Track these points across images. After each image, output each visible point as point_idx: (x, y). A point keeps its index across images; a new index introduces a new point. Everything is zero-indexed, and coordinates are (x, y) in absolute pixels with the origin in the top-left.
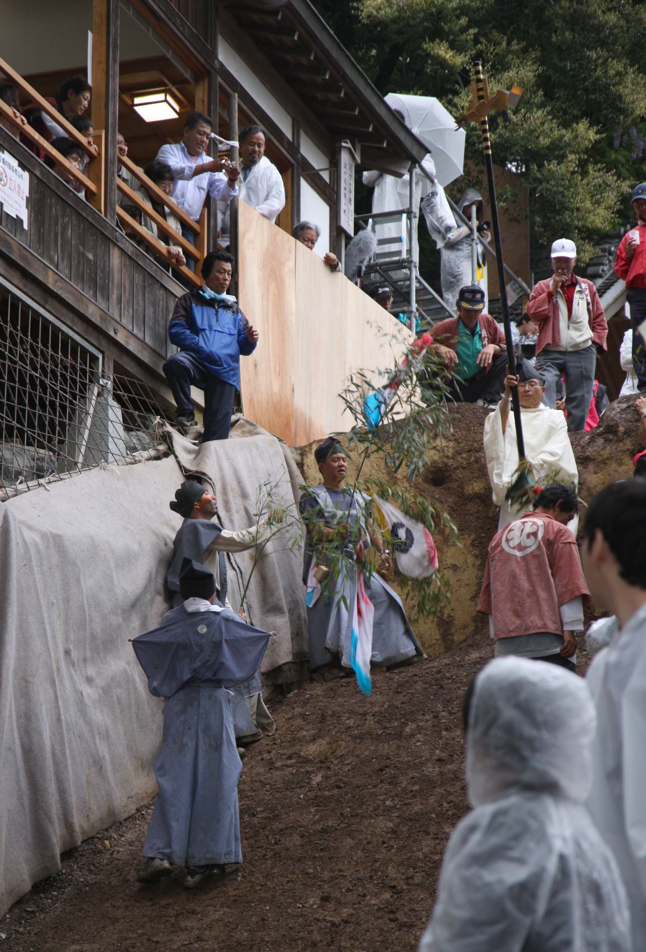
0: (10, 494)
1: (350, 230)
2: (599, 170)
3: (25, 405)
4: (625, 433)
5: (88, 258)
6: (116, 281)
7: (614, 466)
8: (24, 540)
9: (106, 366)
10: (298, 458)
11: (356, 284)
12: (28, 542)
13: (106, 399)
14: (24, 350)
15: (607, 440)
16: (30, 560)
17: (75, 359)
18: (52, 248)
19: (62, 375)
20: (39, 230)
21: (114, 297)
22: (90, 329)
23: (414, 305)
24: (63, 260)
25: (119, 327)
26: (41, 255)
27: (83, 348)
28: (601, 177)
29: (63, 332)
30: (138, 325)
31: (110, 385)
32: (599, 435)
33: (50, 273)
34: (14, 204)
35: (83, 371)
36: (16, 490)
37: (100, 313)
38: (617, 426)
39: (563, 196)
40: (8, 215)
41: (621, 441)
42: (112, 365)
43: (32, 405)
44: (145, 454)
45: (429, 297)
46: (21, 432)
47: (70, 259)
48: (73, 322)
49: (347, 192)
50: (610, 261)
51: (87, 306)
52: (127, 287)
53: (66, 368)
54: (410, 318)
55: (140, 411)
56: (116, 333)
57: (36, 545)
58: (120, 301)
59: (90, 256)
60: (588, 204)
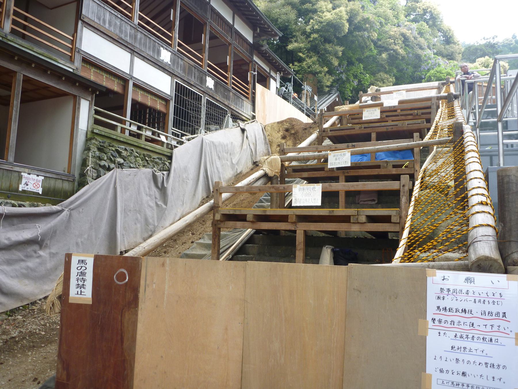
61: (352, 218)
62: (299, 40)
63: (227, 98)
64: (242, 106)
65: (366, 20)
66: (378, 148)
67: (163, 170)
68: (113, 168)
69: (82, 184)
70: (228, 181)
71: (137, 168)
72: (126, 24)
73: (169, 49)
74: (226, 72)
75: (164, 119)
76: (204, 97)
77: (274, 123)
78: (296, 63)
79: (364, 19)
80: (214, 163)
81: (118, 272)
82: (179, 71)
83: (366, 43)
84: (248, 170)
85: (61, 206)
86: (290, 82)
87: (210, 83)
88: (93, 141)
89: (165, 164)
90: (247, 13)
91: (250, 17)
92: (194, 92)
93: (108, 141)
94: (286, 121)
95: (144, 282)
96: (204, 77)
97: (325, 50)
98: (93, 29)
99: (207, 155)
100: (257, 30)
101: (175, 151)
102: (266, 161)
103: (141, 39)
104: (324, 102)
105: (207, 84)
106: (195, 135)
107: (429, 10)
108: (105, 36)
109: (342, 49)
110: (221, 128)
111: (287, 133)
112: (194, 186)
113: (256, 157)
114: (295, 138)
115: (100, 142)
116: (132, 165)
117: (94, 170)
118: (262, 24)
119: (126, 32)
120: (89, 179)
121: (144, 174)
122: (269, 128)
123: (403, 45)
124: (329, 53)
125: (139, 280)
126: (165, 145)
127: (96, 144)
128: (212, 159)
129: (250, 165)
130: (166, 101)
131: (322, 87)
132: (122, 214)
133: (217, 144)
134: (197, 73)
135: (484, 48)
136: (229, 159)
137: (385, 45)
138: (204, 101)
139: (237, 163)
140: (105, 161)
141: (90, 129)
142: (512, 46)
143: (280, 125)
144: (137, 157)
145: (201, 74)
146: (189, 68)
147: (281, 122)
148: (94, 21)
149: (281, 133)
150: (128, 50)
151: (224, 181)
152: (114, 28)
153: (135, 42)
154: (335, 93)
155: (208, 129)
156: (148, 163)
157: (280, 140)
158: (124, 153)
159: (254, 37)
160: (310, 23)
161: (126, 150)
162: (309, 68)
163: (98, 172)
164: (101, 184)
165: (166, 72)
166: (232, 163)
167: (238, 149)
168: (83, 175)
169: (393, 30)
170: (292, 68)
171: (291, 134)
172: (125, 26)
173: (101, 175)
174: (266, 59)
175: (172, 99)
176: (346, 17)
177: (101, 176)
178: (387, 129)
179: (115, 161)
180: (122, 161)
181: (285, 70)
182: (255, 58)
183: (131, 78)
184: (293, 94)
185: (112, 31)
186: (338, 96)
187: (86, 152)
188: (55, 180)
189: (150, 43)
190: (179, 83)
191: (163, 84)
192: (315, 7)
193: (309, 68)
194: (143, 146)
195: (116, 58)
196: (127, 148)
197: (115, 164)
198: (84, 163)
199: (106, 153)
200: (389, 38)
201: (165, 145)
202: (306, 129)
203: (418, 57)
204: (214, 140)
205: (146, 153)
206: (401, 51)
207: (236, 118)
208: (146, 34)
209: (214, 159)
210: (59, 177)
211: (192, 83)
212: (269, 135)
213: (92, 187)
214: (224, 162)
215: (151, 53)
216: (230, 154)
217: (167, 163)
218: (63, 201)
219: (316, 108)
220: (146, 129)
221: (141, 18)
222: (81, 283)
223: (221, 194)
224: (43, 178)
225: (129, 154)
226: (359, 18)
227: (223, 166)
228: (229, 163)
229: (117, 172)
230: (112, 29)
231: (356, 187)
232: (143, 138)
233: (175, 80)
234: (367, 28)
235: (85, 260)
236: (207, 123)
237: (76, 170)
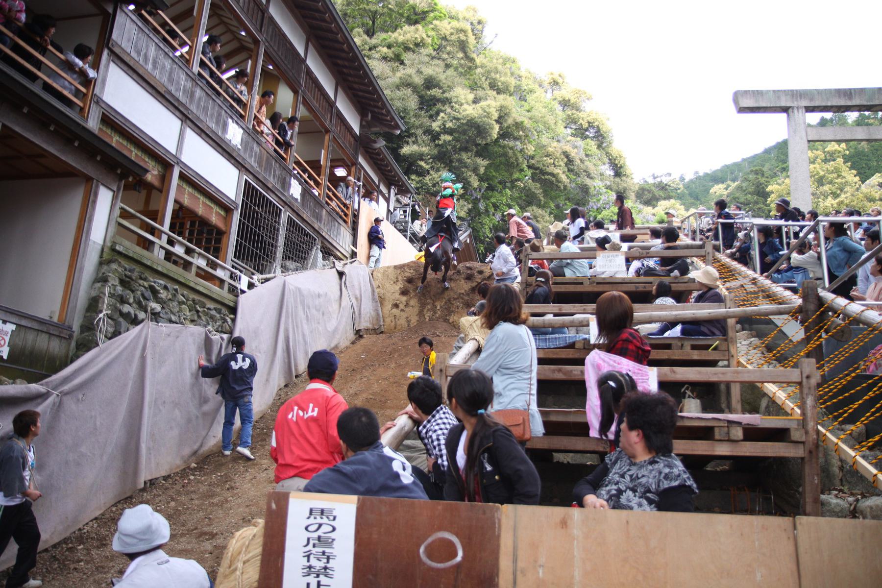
61: (717, 431)
62: (420, 141)
63: (318, 218)
64: (338, 234)
65: (519, 125)
66: (676, 315)
67: (222, 332)
68: (143, 321)
69: (86, 345)
71: (182, 323)
72: (181, 71)
73: (241, 124)
74: (319, 175)
75: (218, 241)
76: (285, 211)
77: (388, 267)
78: (413, 177)
79: (517, 123)
80: (300, 325)
81: (430, 540)
82: (252, 162)
83: (517, 159)
84: (348, 343)
85: (47, 384)
87: (296, 189)
88: (114, 266)
89: (225, 321)
90: (356, 86)
91: (361, 94)
92: (271, 202)
93: (138, 269)
95: (510, 564)
96: (288, 179)
97: (460, 161)
98: (126, 68)
100: (367, 116)
101: (242, 298)
103: (200, 99)
105: (292, 191)
106: (272, 275)
107: (596, 124)
108: (144, 85)
109: (485, 163)
110: (305, 268)
111: (410, 285)
112: (268, 365)
115: (125, 270)
116: (173, 318)
117: (110, 321)
118: (378, 107)
119: (178, 83)
120: (101, 337)
121: (192, 335)
123: (566, 170)
124: (466, 167)
125: (497, 559)
126: (226, 286)
127: (118, 272)
129: (351, 336)
130: (228, 210)
132: (150, 408)
134: (277, 170)
135: (653, 188)
137: (541, 166)
138: (284, 218)
140: (130, 304)
141: (109, 244)
142: (679, 191)
144: (183, 303)
145: (284, 172)
146: (267, 160)
147: (401, 268)
148: (129, 54)
149: (400, 285)
150: (177, 113)
152: (161, 73)
153: (191, 102)
155: (285, 269)
156: (199, 317)
157: (397, 295)
158: (163, 294)
159: (362, 127)
160: (439, 118)
161: (166, 288)
162: (434, 185)
163: (117, 324)
164: (121, 349)
165: (233, 161)
166: (326, 329)
168: (89, 327)
169: (554, 147)
170: (413, 182)
172: (178, 74)
173: (122, 330)
174: (376, 164)
175: (237, 209)
176: (496, 116)
177: (120, 333)
178: (637, 288)
179: (146, 306)
180: (157, 307)
181: (404, 184)
182: (361, 160)
183: (178, 164)
185: (157, 77)
186: (470, 236)
187: (99, 285)
188: (36, 333)
189: (213, 108)
190: (250, 184)
191: (227, 180)
192: (447, 95)
193: (434, 185)
194: (192, 285)
195: (158, 124)
196: (169, 285)
197: (146, 312)
198: (93, 305)
199: (132, 289)
200: (546, 156)
201: (226, 286)
203: (585, 189)
205: (197, 298)
206: (563, 177)
207: (328, 252)
208: (210, 93)
210: (44, 326)
211: (270, 186)
212: (379, 287)
213: (105, 353)
215: (212, 125)
216: (323, 314)
217: (229, 320)
218: (50, 376)
220: (200, 254)
221: (202, 64)
222: (318, 564)
224: (13, 327)
225: (170, 296)
226: (510, 121)
227: (311, 332)
229: (148, 328)
230: (156, 73)
231: (720, 376)
232: (194, 269)
233: (245, 177)
234: (521, 136)
235: (331, 511)
236: (285, 257)
237: (76, 318)
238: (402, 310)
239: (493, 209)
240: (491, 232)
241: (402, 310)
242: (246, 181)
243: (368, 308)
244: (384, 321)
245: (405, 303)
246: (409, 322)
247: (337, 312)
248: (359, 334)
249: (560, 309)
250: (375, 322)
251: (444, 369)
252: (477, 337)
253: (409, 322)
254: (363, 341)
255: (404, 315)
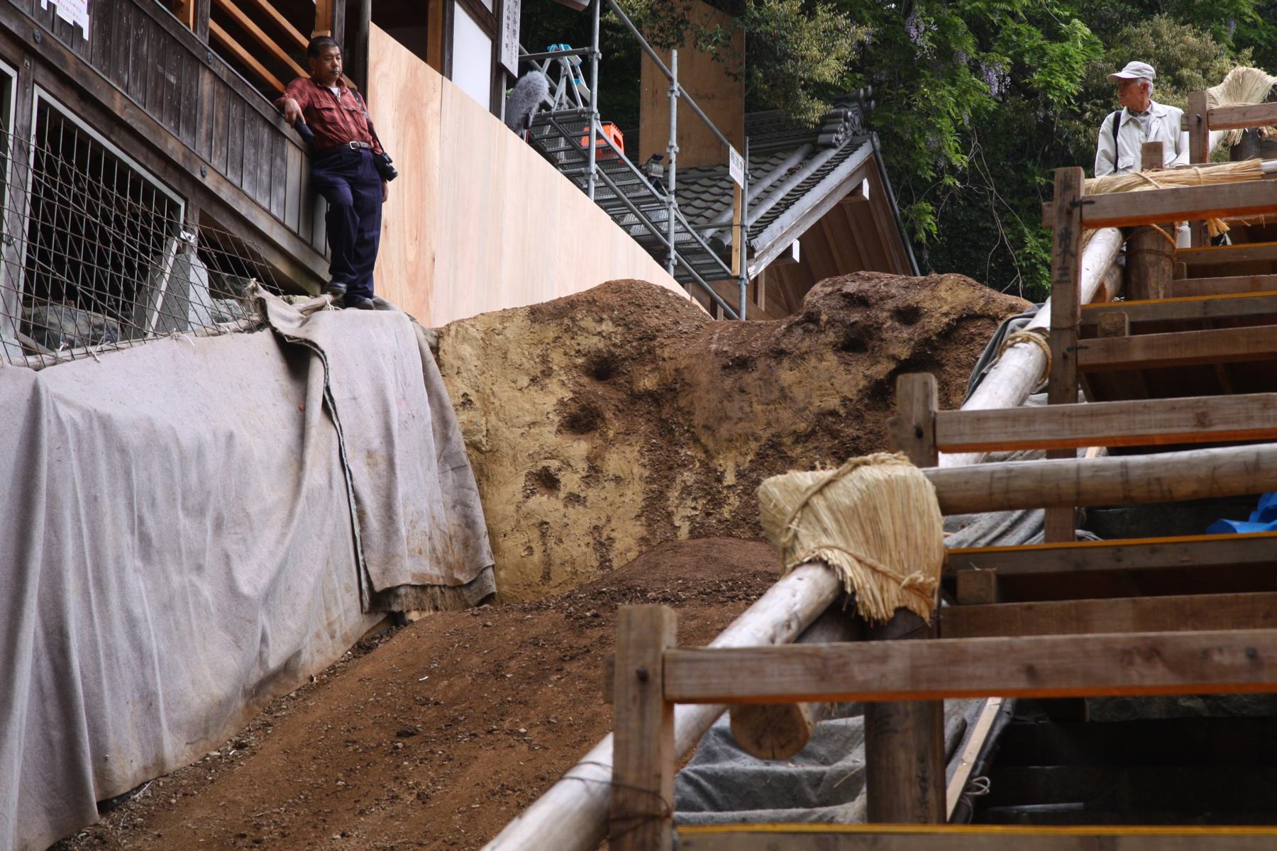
0: (47, 362)
1: (514, 69)
2: (830, 11)
3: (107, 267)
4: (828, 322)
5: (168, 81)
6: (206, 112)
7: (813, 362)
8: (58, 417)
9: (190, 216)
10: (433, 341)
11: (522, 137)
12: (64, 419)
13: (188, 258)
14: (79, 188)
15: (807, 331)
16: (66, 442)
17: (136, 200)
18: (121, 65)
19: (143, 230)
20: (105, 42)
21: (203, 131)
22: (170, 169)
23: (594, 167)
24: (135, 83)
25: (209, 170)
26: (107, 73)
27: (159, 191)
28: (831, 19)
29: (133, 170)
30: (233, 168)
31: (193, 239)
32: (797, 324)
33: (118, 96)
34: (71, 7)
35: (159, 222)
36: (56, 358)
37: (183, 149)
38: (819, 313)
39: (787, 42)
40: (62, 21)
41: (823, 332)
42: (197, 215)
43: (117, 267)
44: (233, 325)
45: (627, 169)
46: (72, 294)
47: (145, 80)
48: (146, 158)
49: (511, 22)
50: (846, 129)
51: (166, 141)
52: (221, 120)
53: (135, 216)
54: (588, 182)
55: (230, 271)
56: (203, 176)
57: (75, 424)
58: (210, 137)
59: (172, 79)
60: (815, 52)
63: (181, 110)
70: (202, 728)
76: (25, 84)
77: (506, 316)
84: (335, 650)
86: (580, 38)
94: (591, 302)
99: (67, 515)
102: (819, 503)
104: (786, 204)
111: (600, 389)
113: (389, 558)
114: (665, 429)
122: (467, 350)
128: (97, 551)
129: (350, 617)
131: (785, 87)
133: (133, 438)
136: (210, 560)
139: (269, 595)
143: (551, 332)
147: (560, 313)
149: (558, 392)
151: (175, 727)
154: (853, 148)
157: (549, 436)
167: (268, 490)
171: (636, 397)
184: (596, 126)
186: (869, 167)
190: (57, 115)
202: (743, 364)
204: (119, 414)
209: (109, 554)
212: (467, 402)
214: (176, 580)
216: (219, 525)
219: (735, 240)
223: (669, 705)
228: (207, 592)
233: (38, 92)
238: (574, 499)
239: (970, 43)
240: (965, 148)
241: (574, 499)
242: (40, 98)
243: (424, 497)
244: (496, 550)
245: (582, 466)
246: (603, 546)
247: (281, 514)
248: (382, 605)
249: (1202, 419)
250: (456, 554)
251: (654, 670)
252: (834, 557)
253: (603, 546)
254: (399, 641)
255: (582, 519)
